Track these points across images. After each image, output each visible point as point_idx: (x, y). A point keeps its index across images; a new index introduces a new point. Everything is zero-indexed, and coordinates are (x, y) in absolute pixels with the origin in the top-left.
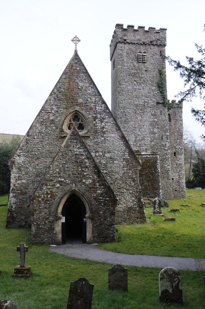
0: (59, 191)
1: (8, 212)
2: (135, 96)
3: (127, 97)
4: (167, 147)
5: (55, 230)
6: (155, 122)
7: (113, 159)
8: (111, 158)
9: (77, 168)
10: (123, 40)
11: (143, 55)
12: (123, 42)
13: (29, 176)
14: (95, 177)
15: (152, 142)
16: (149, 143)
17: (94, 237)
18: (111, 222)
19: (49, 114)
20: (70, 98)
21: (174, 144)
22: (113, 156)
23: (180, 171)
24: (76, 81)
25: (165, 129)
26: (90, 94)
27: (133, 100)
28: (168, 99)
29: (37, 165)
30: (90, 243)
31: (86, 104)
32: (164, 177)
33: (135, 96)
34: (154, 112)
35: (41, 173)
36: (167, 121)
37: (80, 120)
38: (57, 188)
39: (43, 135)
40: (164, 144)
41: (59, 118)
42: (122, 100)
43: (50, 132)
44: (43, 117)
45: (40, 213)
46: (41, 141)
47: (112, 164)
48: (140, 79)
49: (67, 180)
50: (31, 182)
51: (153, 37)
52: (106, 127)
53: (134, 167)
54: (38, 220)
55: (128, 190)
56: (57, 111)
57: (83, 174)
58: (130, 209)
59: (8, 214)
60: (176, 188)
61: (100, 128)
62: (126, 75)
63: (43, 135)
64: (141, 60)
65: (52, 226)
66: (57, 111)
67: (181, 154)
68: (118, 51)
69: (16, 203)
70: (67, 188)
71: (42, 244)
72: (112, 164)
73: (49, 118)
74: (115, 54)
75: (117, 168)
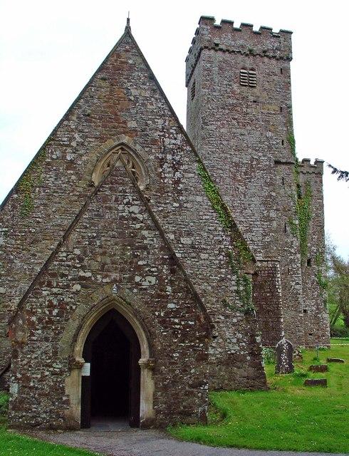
0: (79, 301)
4: (295, 248)
5: (67, 393)
8: (193, 247)
10: (213, 45)
12: (213, 48)
17: (158, 412)
20: (110, 118)
24: (125, 86)
28: (297, 156)
30: (148, 425)
38: (73, 293)
41: (84, 158)
43: (65, 185)
44: (52, 153)
45: (33, 352)
46: (45, 205)
49: (99, 276)
50: (18, 293)
51: (269, 44)
55: (227, 317)
56: (82, 144)
58: (231, 360)
64: (247, 81)
66: (82, 144)
68: (201, 63)
70: (98, 297)
71: (33, 427)
73: (64, 157)
74: (196, 71)
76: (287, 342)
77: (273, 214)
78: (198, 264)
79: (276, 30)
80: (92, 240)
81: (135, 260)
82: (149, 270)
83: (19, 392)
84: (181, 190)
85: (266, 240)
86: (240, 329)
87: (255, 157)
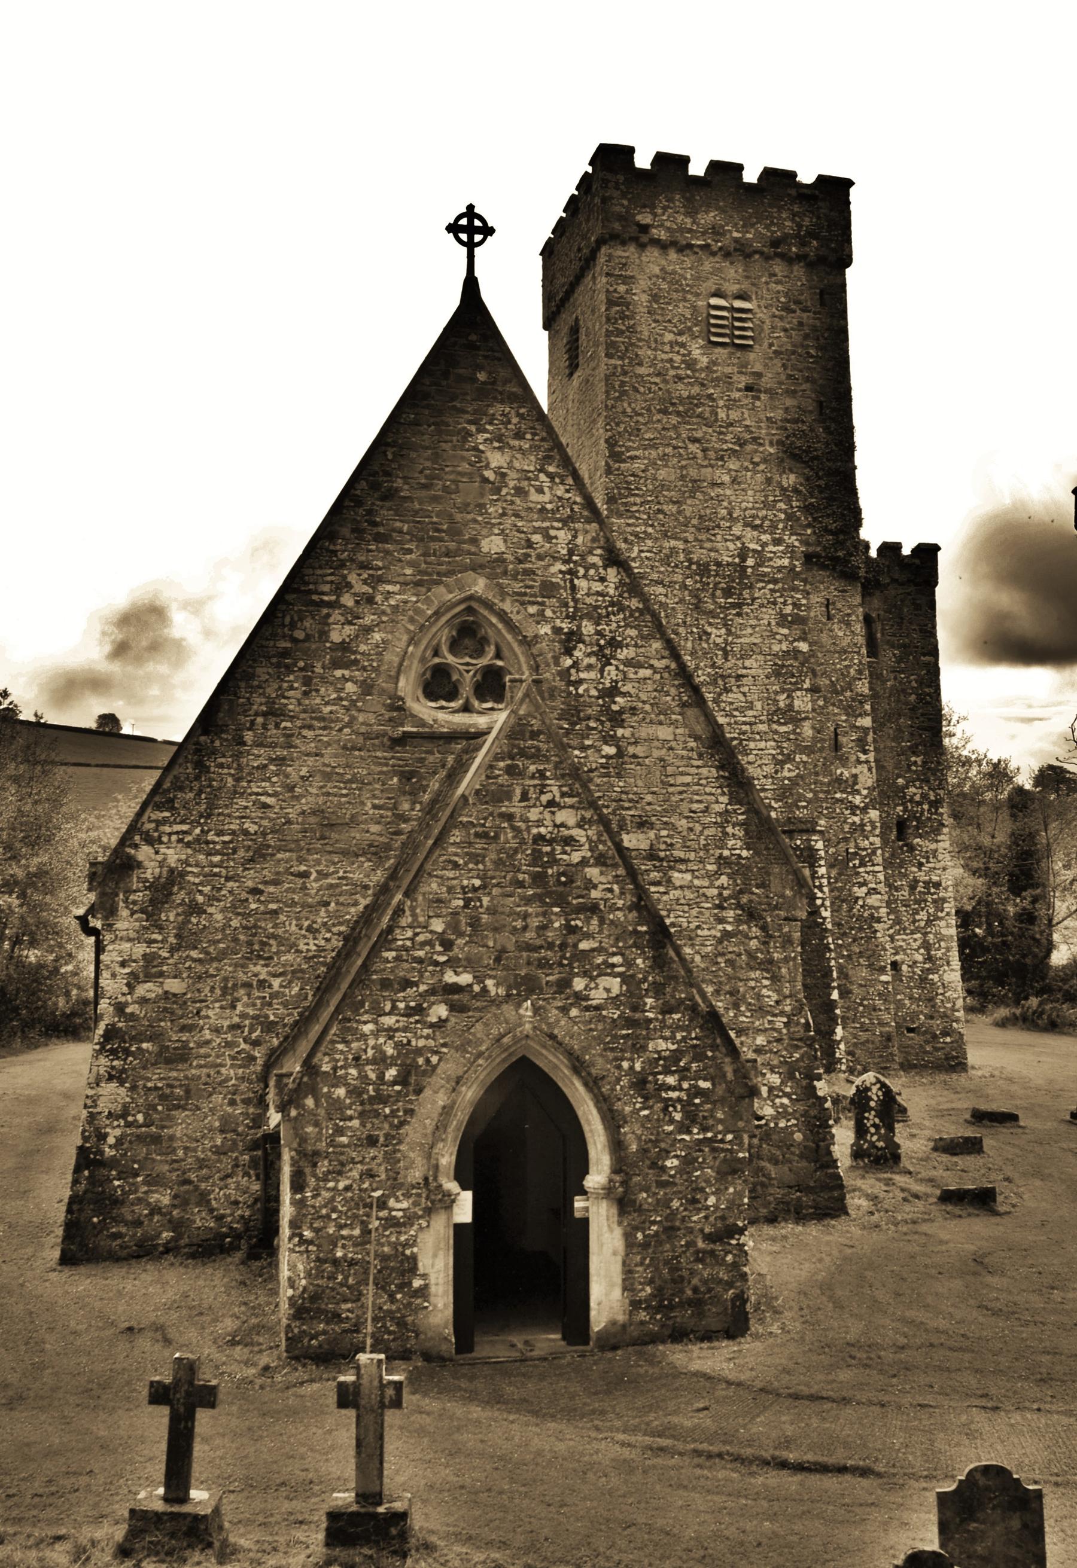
0: (444, 1045)
1: (77, 1170)
2: (695, 522)
3: (652, 526)
4: (865, 792)
6: (801, 658)
7: (661, 860)
8: (652, 855)
9: (544, 914)
11: (733, 309)
12: (635, 240)
13: (207, 953)
14: (639, 961)
15: (782, 763)
16: (769, 769)
17: (635, 1305)
18: (723, 1218)
19: (325, 611)
21: (899, 776)
22: (663, 847)
23: (929, 922)
25: (848, 694)
26: (543, 510)
27: (686, 541)
29: (255, 891)
31: (520, 562)
32: (849, 957)
33: (695, 522)
34: (794, 605)
35: (274, 936)
36: (858, 653)
37: (491, 650)
38: (432, 1026)
39: (289, 724)
40: (846, 774)
41: (377, 636)
42: (626, 541)
43: (329, 708)
44: (293, 626)
46: (281, 761)
47: (662, 889)
48: (721, 433)
49: (490, 983)
50: (218, 992)
52: (627, 688)
53: (776, 907)
54: (324, 1211)
57: (575, 946)
59: (75, 1182)
60: (914, 1016)
61: (594, 692)
62: (649, 410)
63: (289, 724)
65: (406, 1245)
67: (937, 831)
69: (124, 1114)
72: (662, 889)
75: (686, 908)
76: (878, 1081)
77: (802, 702)
78: (665, 898)
79: (806, 177)
80: (470, 896)
81: (571, 940)
82: (605, 962)
83: (308, 1275)
84: (621, 712)
85: (786, 774)
86: (775, 1062)
87: (752, 546)
